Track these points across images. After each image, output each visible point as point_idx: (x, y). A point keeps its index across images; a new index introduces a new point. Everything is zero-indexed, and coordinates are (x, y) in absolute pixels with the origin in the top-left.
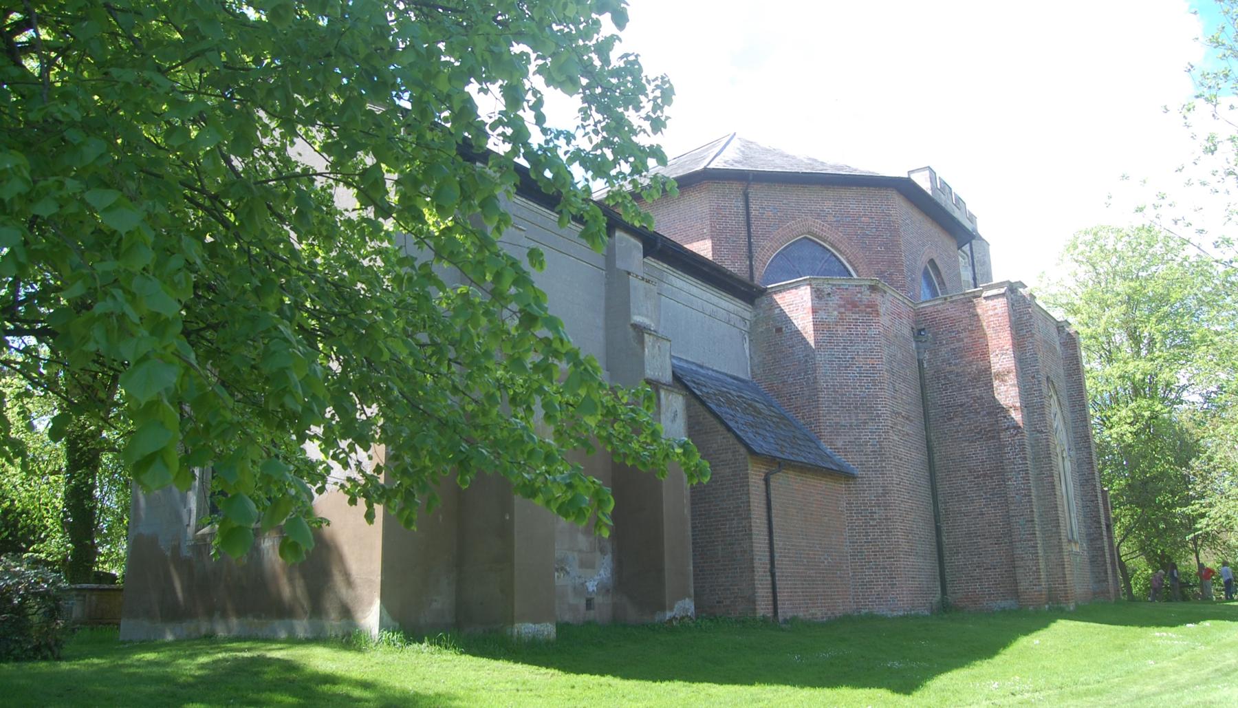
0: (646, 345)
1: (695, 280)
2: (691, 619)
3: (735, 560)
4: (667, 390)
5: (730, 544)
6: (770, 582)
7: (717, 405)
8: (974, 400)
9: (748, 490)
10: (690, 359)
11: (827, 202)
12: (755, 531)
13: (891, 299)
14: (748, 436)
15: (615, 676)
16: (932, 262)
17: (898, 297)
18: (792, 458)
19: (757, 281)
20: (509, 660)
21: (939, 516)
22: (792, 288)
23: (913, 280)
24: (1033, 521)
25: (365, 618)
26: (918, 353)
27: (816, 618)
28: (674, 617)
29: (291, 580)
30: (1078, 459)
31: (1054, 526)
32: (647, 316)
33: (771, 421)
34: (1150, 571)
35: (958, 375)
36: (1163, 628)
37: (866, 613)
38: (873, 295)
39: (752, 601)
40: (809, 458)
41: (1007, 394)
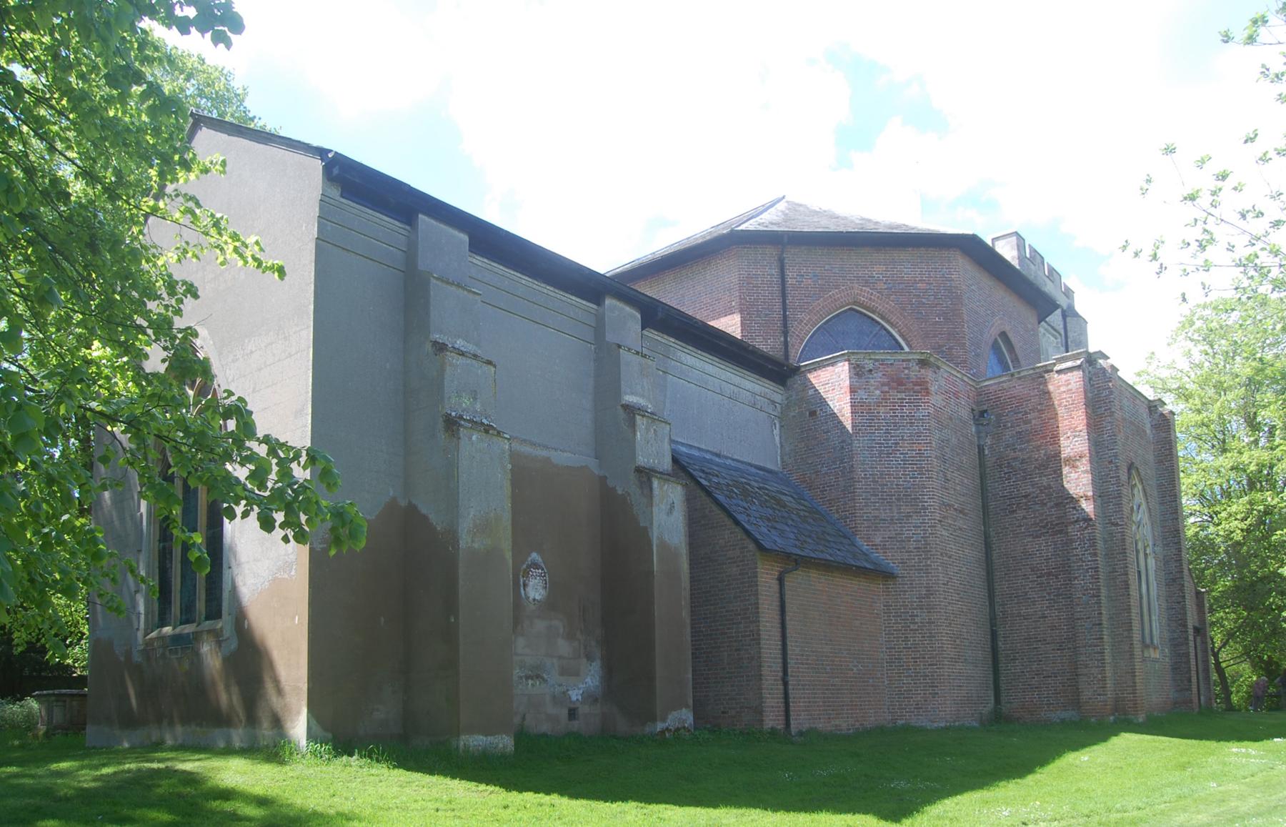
0: (637, 428)
1: (711, 357)
2: (689, 731)
3: (741, 667)
4: (660, 478)
5: (736, 650)
6: (782, 691)
7: (727, 496)
8: (1041, 490)
9: (757, 590)
10: (703, 446)
11: (878, 267)
12: (764, 635)
13: (945, 375)
14: (762, 531)
15: (562, 794)
16: (1003, 335)
17: (955, 373)
18: (814, 556)
19: (793, 361)
20: (445, 775)
21: (995, 619)
22: (828, 365)
23: (977, 355)
24: (1100, 624)
25: (294, 728)
26: (979, 437)
27: (841, 730)
28: (667, 729)
29: (227, 687)
30: (1165, 556)
31: (1127, 630)
32: (643, 396)
33: (798, 514)
34: (1255, 678)
35: (1023, 462)
36: (1246, 743)
37: (903, 725)
38: (923, 371)
39: (759, 711)
40: (837, 555)
41: (1078, 482)
